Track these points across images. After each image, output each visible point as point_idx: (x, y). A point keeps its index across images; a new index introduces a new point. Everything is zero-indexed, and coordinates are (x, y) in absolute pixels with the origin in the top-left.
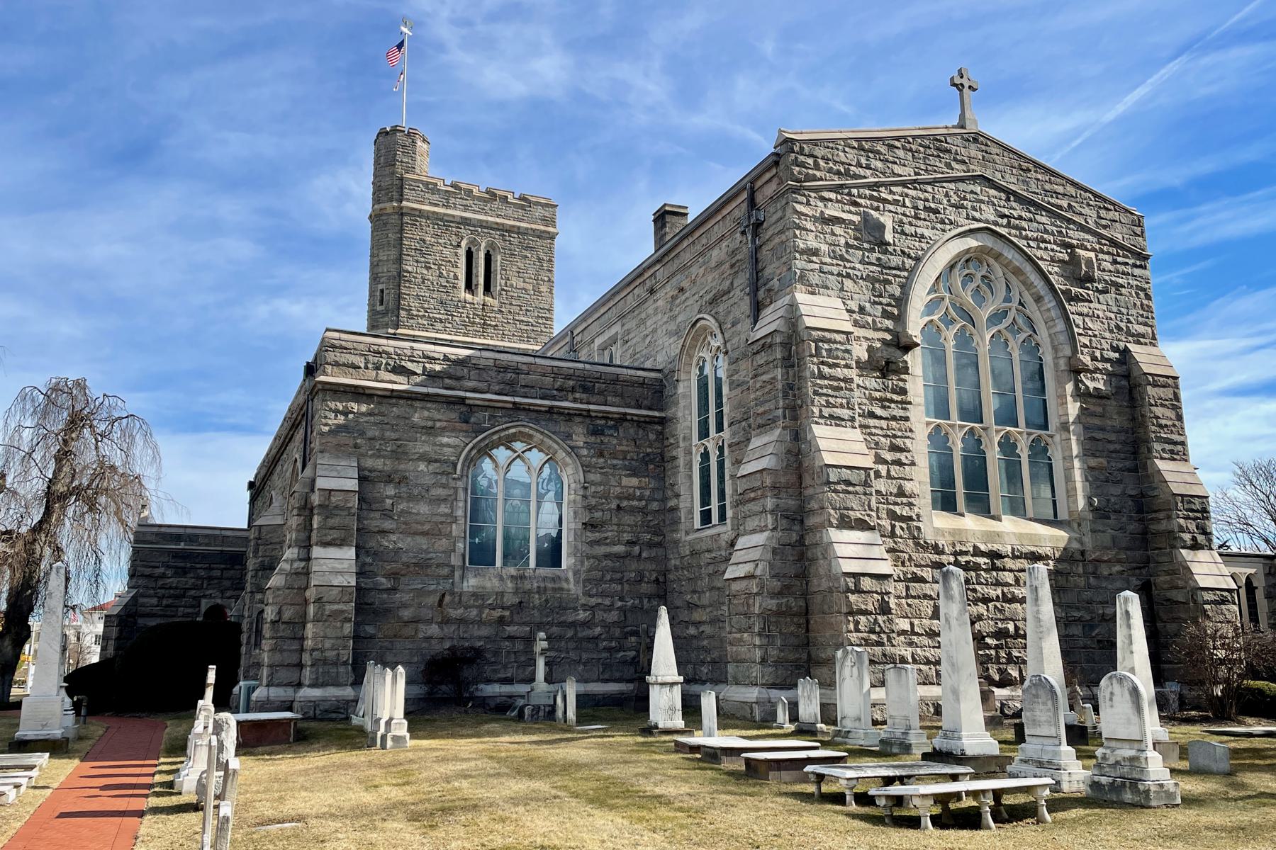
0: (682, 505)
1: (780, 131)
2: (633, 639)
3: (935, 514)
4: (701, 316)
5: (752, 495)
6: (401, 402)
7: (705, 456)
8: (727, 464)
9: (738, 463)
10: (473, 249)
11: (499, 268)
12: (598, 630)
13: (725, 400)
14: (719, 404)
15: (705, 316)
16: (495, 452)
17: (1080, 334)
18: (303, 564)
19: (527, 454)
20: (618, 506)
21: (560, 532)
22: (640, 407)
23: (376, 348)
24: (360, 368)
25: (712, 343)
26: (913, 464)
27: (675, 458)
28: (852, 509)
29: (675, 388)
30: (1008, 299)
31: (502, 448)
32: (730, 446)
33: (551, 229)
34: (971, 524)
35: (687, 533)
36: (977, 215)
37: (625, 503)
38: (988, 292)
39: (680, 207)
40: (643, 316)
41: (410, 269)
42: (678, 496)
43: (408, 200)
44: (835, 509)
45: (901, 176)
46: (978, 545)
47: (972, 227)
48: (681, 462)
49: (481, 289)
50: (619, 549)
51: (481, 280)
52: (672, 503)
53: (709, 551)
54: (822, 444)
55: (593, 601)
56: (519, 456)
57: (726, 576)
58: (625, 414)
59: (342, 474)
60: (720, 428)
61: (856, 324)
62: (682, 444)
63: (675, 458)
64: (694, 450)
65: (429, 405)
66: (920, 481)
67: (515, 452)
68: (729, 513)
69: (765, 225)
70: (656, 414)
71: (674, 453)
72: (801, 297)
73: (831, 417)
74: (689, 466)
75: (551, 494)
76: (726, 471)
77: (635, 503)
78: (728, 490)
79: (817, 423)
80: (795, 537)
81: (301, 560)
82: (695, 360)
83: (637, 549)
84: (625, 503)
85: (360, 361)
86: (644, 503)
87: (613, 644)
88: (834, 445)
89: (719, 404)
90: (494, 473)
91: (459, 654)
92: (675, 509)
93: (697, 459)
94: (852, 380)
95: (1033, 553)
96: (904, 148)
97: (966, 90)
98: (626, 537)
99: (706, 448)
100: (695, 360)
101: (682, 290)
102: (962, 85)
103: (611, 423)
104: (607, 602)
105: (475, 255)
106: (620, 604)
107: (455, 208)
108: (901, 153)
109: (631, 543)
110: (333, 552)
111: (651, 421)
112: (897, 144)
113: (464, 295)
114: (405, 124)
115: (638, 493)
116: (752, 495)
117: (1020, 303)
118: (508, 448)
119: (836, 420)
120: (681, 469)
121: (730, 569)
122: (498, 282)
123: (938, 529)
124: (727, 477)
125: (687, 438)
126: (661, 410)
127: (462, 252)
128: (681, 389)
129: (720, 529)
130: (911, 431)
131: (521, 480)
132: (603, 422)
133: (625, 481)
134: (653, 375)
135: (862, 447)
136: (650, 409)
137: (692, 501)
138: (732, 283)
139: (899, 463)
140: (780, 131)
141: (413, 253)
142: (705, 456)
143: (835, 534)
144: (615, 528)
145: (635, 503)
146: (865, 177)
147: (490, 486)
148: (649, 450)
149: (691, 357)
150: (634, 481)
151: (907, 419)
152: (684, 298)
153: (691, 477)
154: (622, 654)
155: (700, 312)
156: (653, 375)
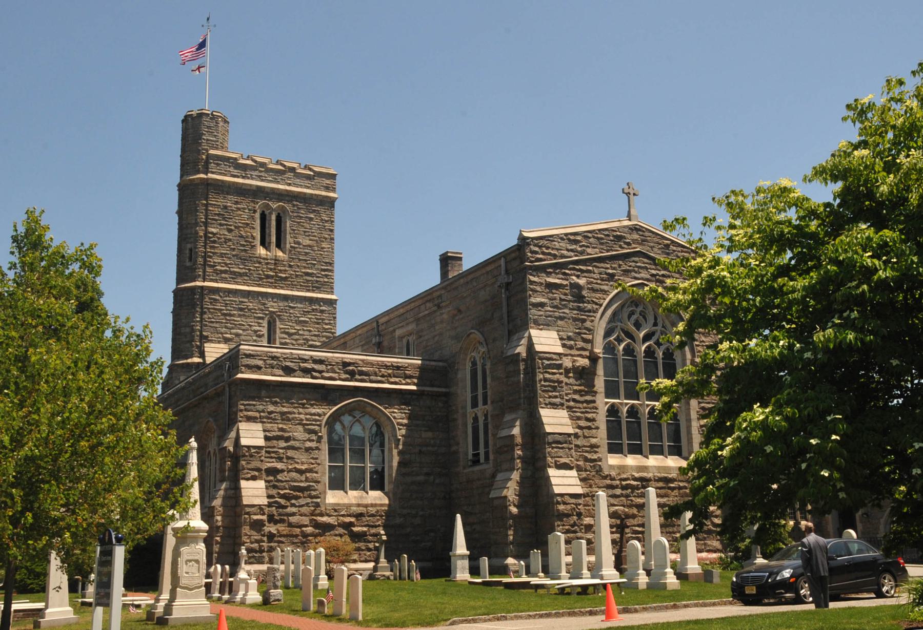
0: (460, 450)
1: (521, 231)
2: (432, 534)
3: (611, 457)
4: (473, 331)
5: (506, 449)
6: (286, 388)
7: (476, 419)
8: (490, 426)
9: (498, 427)
10: (267, 212)
11: (288, 229)
12: (408, 530)
13: (488, 386)
14: (485, 387)
15: (476, 332)
16: (342, 418)
17: (698, 346)
18: (233, 492)
19: (362, 420)
20: (420, 451)
21: (383, 468)
22: (432, 386)
23: (270, 354)
24: (261, 368)
25: (480, 348)
26: (597, 428)
27: (455, 420)
28: (561, 457)
29: (456, 374)
30: (655, 324)
31: (347, 415)
32: (492, 416)
33: (332, 195)
34: (631, 460)
35: (464, 468)
36: (637, 275)
37: (424, 449)
38: (643, 320)
39: (457, 253)
40: (433, 322)
41: (214, 230)
42: (458, 444)
43: (213, 173)
44: (552, 457)
45: (591, 254)
46: (634, 474)
47: (634, 283)
48: (460, 422)
49: (273, 245)
50: (421, 478)
51: (274, 239)
52: (454, 448)
53: (479, 479)
54: (545, 420)
55: (405, 511)
56: (357, 420)
57: (491, 496)
58: (424, 391)
59: (254, 436)
60: (485, 403)
61: (564, 346)
62: (460, 411)
63: (455, 420)
64: (468, 415)
65: (303, 390)
66: (601, 436)
67: (355, 417)
68: (491, 457)
69: (512, 285)
70: (443, 390)
71: (455, 416)
72: (534, 332)
73: (550, 403)
74: (465, 425)
75: (378, 444)
76: (490, 431)
77: (430, 448)
78: (491, 443)
79: (542, 408)
80: (529, 473)
81: (232, 489)
82: (468, 358)
83: (432, 478)
84: (424, 449)
85: (260, 363)
86: (436, 448)
87: (418, 538)
88: (551, 421)
89: (485, 387)
90: (342, 431)
91: (703, 440)
92: (456, 452)
93: (470, 422)
94: (562, 382)
95: (666, 478)
96: (594, 237)
97: (631, 196)
98: (425, 470)
99: (476, 414)
100: (468, 358)
101: (460, 311)
102: (629, 193)
103: (414, 397)
104: (414, 512)
105: (267, 218)
106: (421, 513)
107: (252, 179)
108: (592, 240)
109: (428, 474)
110: (251, 484)
111: (439, 395)
112: (590, 235)
113: (262, 251)
114: (208, 109)
115: (432, 442)
116: (506, 449)
117: (663, 327)
118: (350, 415)
119: (554, 406)
120: (460, 427)
121: (492, 492)
122: (289, 241)
123: (611, 466)
124: (490, 435)
125: (464, 407)
126: (446, 387)
127: (258, 215)
128: (459, 376)
129: (485, 466)
130: (596, 408)
131: (359, 435)
132: (410, 396)
133: (424, 435)
134: (441, 364)
135: (568, 421)
136: (439, 387)
137: (467, 447)
138: (493, 315)
139: (589, 428)
140: (521, 231)
141: (217, 218)
142: (476, 419)
143: (552, 472)
144: (418, 465)
145: (430, 448)
146: (570, 257)
147: (340, 440)
148: (439, 414)
149: (466, 355)
150: (430, 434)
151: (594, 402)
152: (461, 316)
153: (466, 432)
154: (423, 544)
155: (472, 328)
156: (441, 364)
